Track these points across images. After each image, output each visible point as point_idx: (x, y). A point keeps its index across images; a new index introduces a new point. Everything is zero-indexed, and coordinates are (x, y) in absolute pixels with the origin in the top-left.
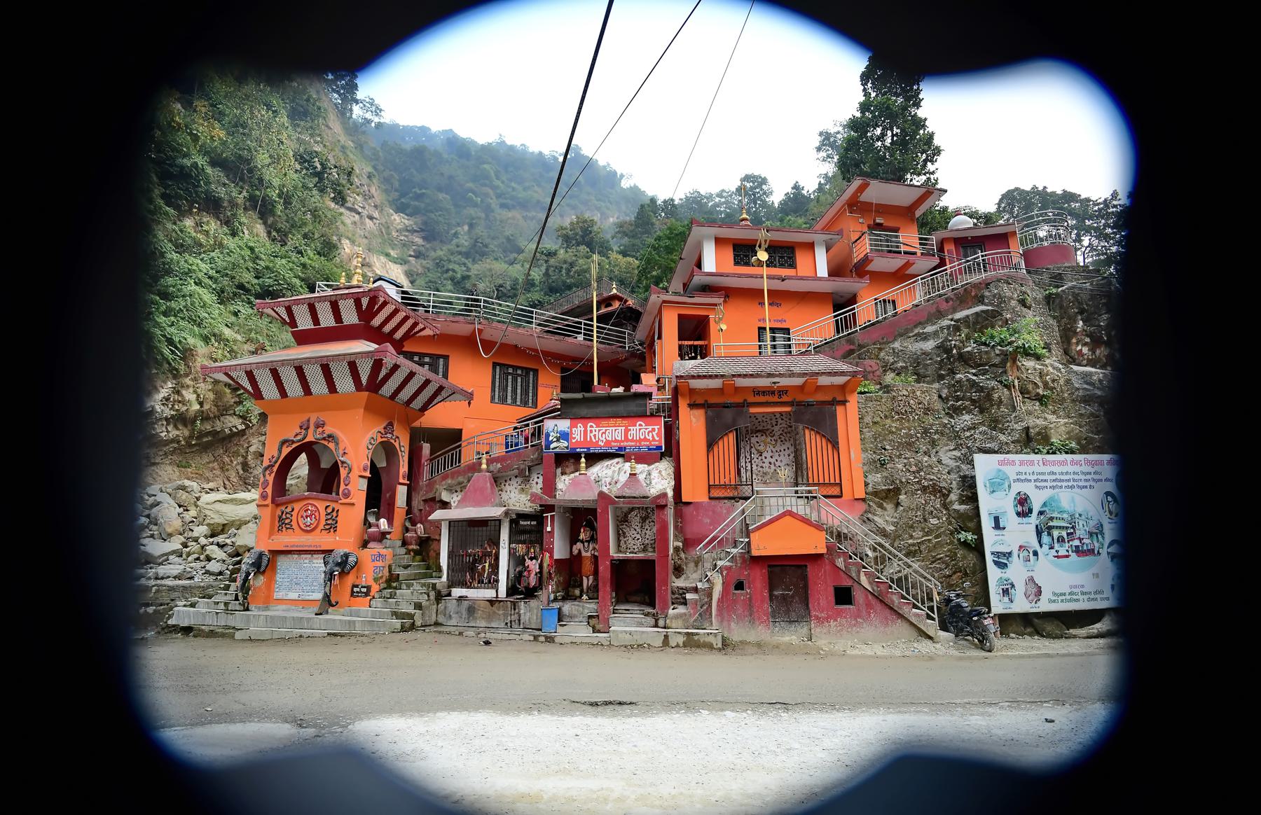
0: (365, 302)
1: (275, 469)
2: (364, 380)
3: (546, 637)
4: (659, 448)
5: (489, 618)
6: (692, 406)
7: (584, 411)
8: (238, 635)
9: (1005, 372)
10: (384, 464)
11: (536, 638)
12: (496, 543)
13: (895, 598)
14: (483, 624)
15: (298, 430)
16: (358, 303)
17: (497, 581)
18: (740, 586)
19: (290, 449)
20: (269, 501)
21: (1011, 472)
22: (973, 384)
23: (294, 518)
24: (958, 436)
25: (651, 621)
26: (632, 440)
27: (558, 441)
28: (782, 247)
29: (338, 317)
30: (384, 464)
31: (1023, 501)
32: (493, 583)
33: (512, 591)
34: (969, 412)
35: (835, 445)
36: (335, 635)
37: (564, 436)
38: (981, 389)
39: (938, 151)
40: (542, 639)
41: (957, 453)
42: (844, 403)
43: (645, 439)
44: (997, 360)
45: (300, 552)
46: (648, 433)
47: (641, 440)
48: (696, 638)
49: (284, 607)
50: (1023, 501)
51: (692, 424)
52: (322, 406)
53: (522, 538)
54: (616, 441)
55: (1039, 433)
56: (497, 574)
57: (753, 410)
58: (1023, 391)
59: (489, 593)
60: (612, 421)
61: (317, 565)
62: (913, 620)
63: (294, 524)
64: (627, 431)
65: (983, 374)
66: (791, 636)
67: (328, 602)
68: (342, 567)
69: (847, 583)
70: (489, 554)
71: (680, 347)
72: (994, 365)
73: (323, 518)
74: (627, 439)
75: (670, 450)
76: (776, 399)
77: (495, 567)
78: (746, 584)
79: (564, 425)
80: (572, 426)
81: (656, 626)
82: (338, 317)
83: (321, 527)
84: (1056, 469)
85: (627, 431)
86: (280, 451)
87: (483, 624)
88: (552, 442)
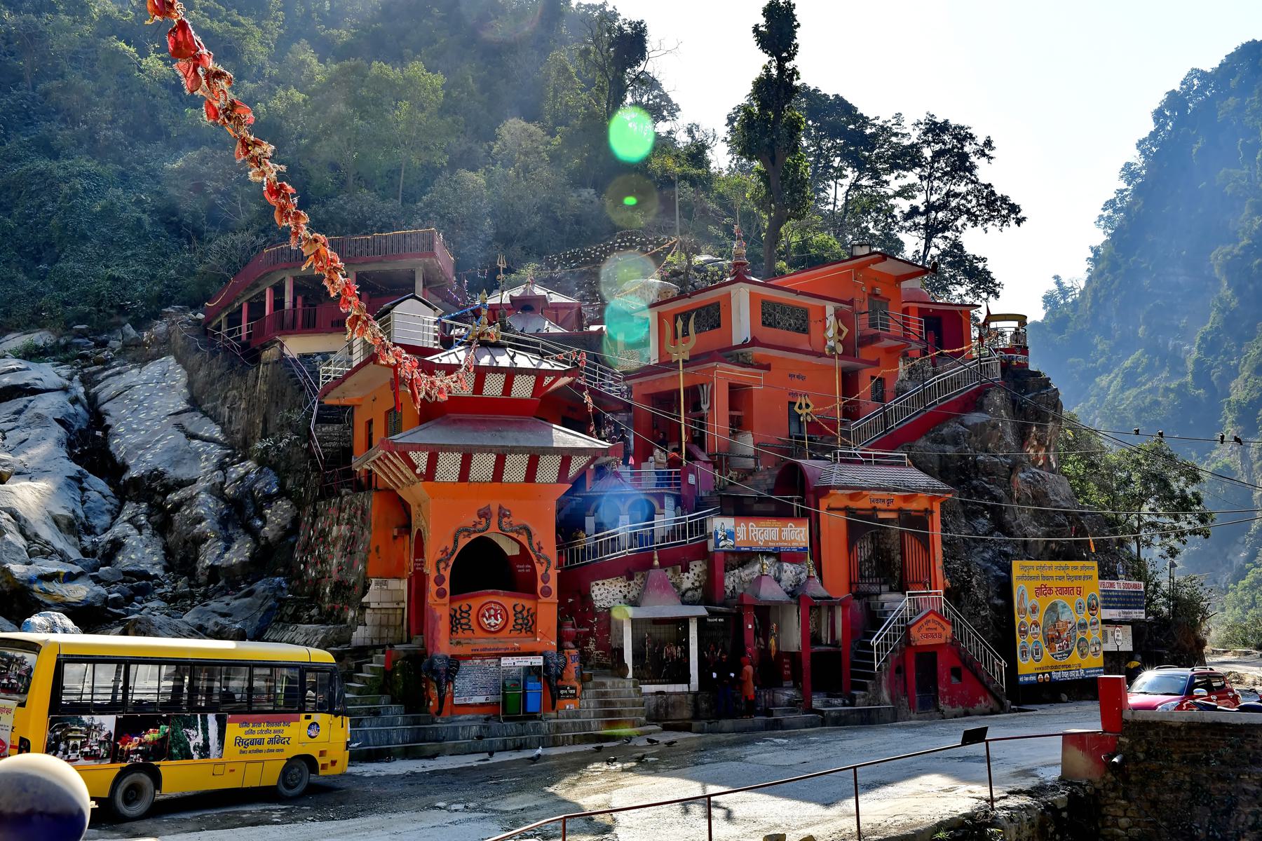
15: (477, 519)
19: (468, 540)
30: (517, 552)
32: (686, 679)
37: (730, 535)
43: (795, 541)
64: (781, 531)
71: (731, 417)
73: (512, 619)
79: (729, 523)
83: (510, 626)
85: (781, 531)
86: (456, 541)
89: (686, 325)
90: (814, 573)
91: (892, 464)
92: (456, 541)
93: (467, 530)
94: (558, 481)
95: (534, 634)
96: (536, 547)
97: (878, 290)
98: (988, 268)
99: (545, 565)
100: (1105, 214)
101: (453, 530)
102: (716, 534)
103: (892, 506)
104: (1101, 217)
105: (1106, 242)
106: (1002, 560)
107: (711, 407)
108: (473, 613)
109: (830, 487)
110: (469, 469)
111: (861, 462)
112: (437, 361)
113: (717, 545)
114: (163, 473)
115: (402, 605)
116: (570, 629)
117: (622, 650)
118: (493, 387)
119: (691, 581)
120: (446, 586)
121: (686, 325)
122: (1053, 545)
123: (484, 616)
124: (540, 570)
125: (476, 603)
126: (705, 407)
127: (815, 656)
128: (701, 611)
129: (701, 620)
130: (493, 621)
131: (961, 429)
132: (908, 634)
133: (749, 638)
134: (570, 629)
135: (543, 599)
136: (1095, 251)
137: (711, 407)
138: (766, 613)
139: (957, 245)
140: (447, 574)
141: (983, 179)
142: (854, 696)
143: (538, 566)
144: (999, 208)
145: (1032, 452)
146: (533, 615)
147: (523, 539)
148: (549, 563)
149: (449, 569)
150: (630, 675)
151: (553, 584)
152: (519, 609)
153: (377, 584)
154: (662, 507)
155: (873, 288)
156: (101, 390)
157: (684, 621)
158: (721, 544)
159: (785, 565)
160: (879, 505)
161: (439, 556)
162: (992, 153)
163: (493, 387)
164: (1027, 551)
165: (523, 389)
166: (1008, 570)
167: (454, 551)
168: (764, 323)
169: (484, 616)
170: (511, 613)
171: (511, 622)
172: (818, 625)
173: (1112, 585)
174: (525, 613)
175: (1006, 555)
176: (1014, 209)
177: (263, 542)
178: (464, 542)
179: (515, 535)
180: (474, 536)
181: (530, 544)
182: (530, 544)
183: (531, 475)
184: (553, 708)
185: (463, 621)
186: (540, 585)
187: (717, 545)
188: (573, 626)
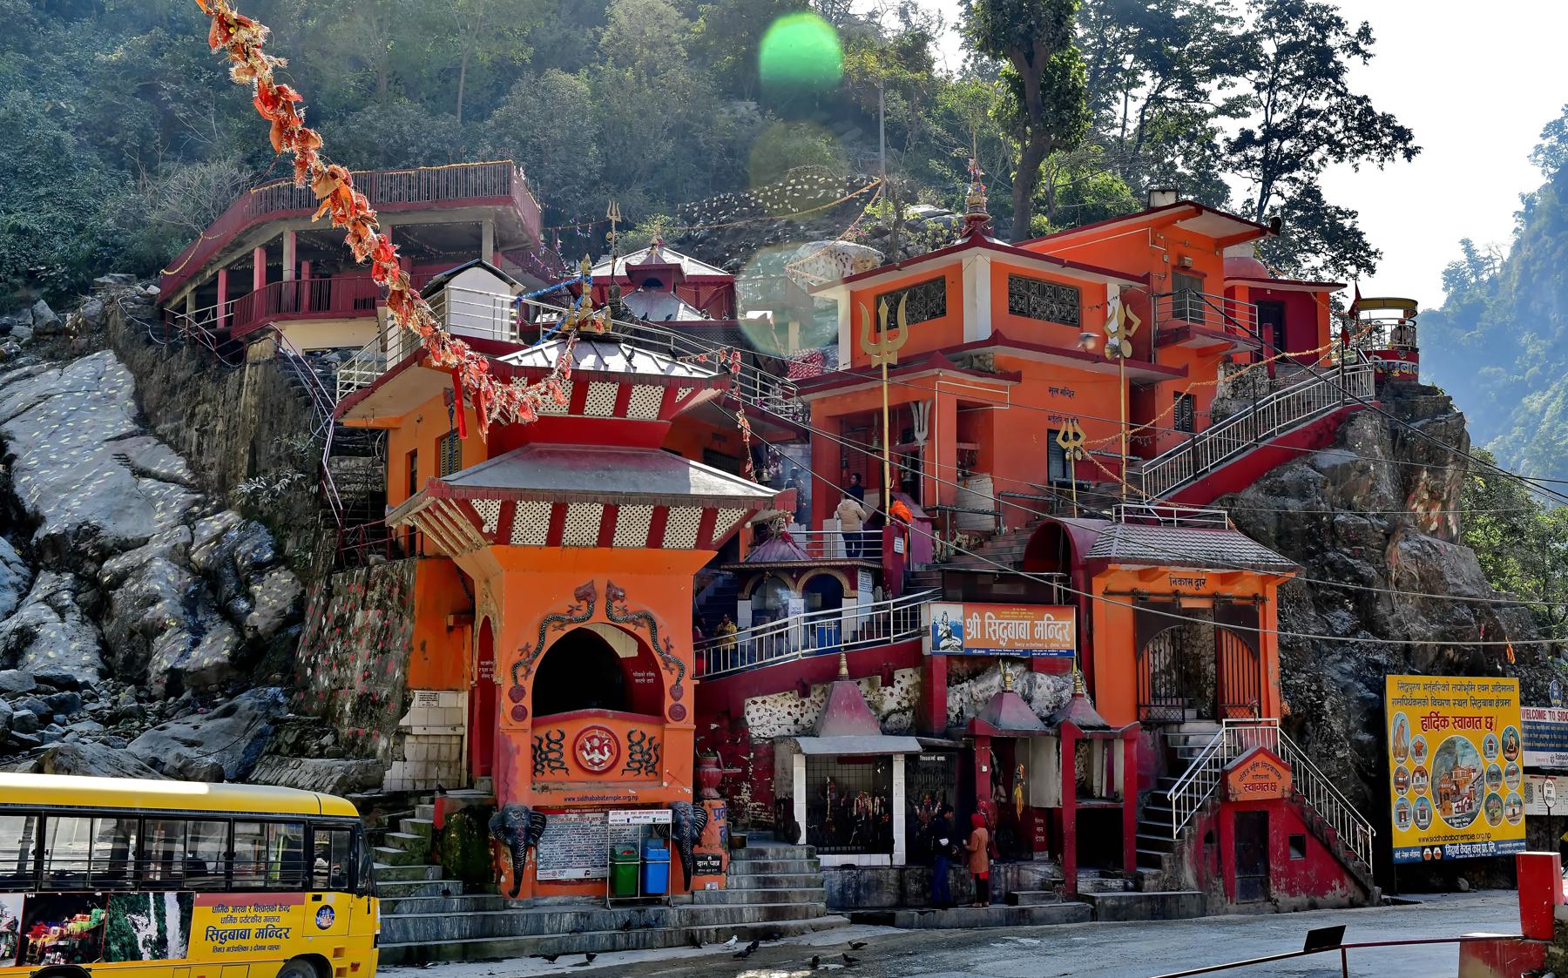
1: (534, 668)
15: (575, 603)
19: (560, 634)
23: (567, 750)
26: (1039, 641)
27: (949, 636)
37: (956, 630)
42: (1263, 600)
54: (1021, 640)
64: (1033, 626)
74: (1033, 639)
85: (1033, 626)
86: (542, 635)
89: (893, 312)
90: (1082, 690)
91: (1204, 527)
92: (542, 635)
93: (558, 619)
94: (697, 546)
95: (659, 776)
96: (662, 646)
97: (1188, 261)
98: (1360, 227)
99: (676, 673)
100: (1546, 143)
101: (537, 618)
102: (935, 628)
103: (1202, 590)
104: (1539, 148)
105: (1546, 186)
106: (1370, 674)
107: (930, 437)
108: (567, 744)
109: (1108, 560)
111: (1158, 523)
112: (514, 363)
113: (936, 646)
114: (97, 529)
115: (460, 731)
117: (789, 803)
118: (600, 403)
120: (527, 702)
121: (893, 312)
122: (1451, 652)
123: (583, 748)
124: (669, 680)
126: (920, 436)
127: (1082, 814)
128: (912, 744)
129: (911, 758)
130: (596, 756)
132: (1223, 777)
133: (983, 786)
135: (672, 724)
136: (1529, 201)
137: (930, 437)
138: (1008, 749)
139: (1312, 192)
140: (528, 684)
141: (1355, 89)
143: (665, 673)
144: (1378, 133)
145: (1420, 509)
146: (658, 748)
147: (644, 632)
148: (682, 670)
149: (531, 677)
151: (688, 701)
152: (636, 738)
153: (422, 699)
154: (854, 587)
155: (1181, 257)
157: (886, 760)
158: (942, 644)
160: (1184, 588)
161: (516, 657)
162: (1370, 49)
163: (600, 403)
164: (1408, 660)
165: (644, 406)
166: (1380, 688)
167: (538, 650)
168: (1012, 310)
169: (583, 748)
170: (625, 744)
171: (625, 758)
172: (1088, 768)
173: (1541, 715)
174: (645, 745)
175: (1377, 666)
176: (1402, 135)
177: (249, 635)
178: (553, 636)
180: (568, 628)
181: (654, 641)
182: (654, 641)
183: (656, 537)
184: (687, 888)
186: (668, 702)
187: (936, 646)
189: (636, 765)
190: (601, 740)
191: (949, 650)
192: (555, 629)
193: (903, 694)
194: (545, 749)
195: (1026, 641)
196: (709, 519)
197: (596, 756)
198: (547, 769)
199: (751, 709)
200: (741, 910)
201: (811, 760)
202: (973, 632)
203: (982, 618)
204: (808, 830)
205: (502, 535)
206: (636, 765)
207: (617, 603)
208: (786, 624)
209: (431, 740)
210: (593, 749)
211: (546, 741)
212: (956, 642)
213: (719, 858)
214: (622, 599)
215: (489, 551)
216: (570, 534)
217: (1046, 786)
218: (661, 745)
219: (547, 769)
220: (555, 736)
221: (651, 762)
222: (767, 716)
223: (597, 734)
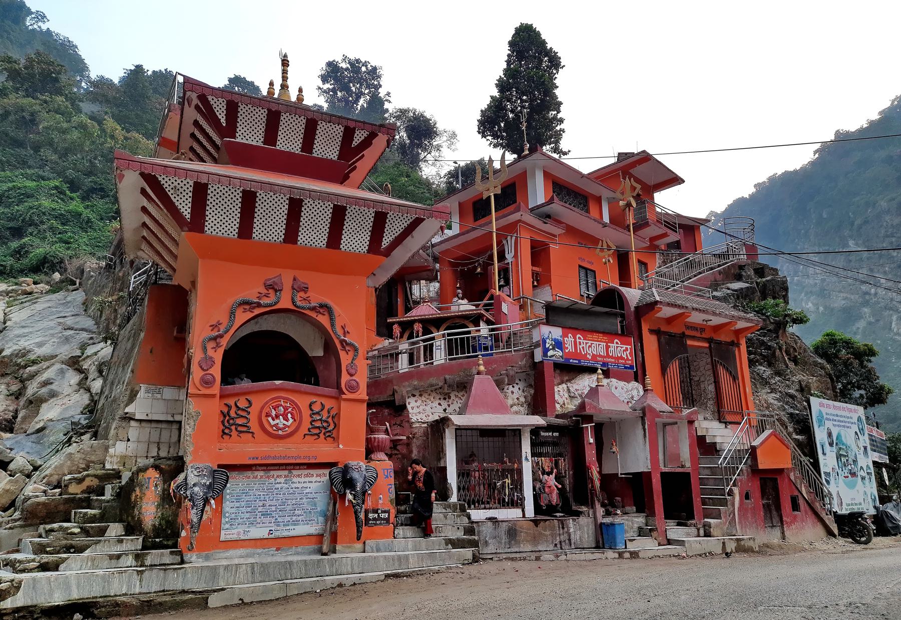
0: (359, 137)
1: (225, 342)
2: (386, 242)
3: (631, 553)
4: (631, 367)
5: (535, 539)
6: (652, 331)
7: (570, 322)
8: (214, 601)
9: (777, 337)
10: (320, 353)
11: (621, 555)
12: (517, 456)
13: (817, 504)
14: (529, 548)
15: (264, 291)
16: (349, 133)
17: (522, 499)
18: (747, 497)
20: (216, 389)
21: (824, 410)
22: (763, 343)
24: (767, 383)
25: (693, 530)
26: (612, 357)
27: (553, 349)
28: (580, 195)
29: (271, 135)
30: (320, 353)
31: (830, 435)
32: (518, 503)
33: (538, 509)
34: (761, 364)
35: (735, 378)
36: (396, 576)
37: (558, 345)
38: (769, 348)
39: (374, 73)
40: (627, 555)
41: (773, 395)
42: (738, 345)
43: (622, 358)
44: (771, 327)
45: (267, 467)
46: (621, 350)
47: (618, 358)
48: (742, 543)
49: (241, 551)
50: (830, 435)
51: (651, 343)
52: (311, 261)
53: (544, 450)
54: (600, 356)
55: (806, 386)
56: (521, 490)
57: (689, 342)
58: (788, 353)
59: (513, 514)
60: (595, 336)
61: (313, 485)
62: (827, 522)
63: (254, 425)
64: (608, 347)
65: (764, 336)
66: (773, 537)
67: (327, 542)
68: (343, 483)
69: (796, 493)
70: (511, 471)
72: (769, 331)
74: (608, 356)
75: (638, 374)
76: (698, 334)
77: (518, 485)
78: (751, 495)
79: (556, 332)
80: (565, 335)
81: (699, 536)
82: (271, 135)
83: (304, 430)
84: (839, 413)
85: (608, 347)
86: (232, 314)
87: (529, 548)
88: (548, 350)
92: (232, 314)
94: (369, 251)
95: (336, 440)
96: (339, 332)
99: (351, 353)
101: (231, 301)
102: (544, 342)
103: (704, 336)
107: (516, 256)
108: (254, 411)
110: (251, 223)
114: (29, 351)
116: (382, 436)
117: (445, 468)
118: (289, 140)
119: (515, 396)
120: (216, 371)
123: (268, 415)
124: (345, 358)
125: (258, 402)
126: (509, 257)
127: (663, 474)
128: (538, 420)
129: (535, 431)
130: (281, 422)
131: (729, 292)
134: (382, 436)
140: (218, 357)
142: (709, 526)
143: (342, 354)
147: (324, 320)
148: (356, 350)
149: (221, 351)
150: (454, 499)
151: (362, 378)
152: (316, 408)
153: (147, 392)
156: (310, 554)
157: (515, 433)
158: (550, 353)
159: (614, 381)
160: (688, 332)
169: (268, 415)
170: (306, 413)
171: (306, 425)
179: (313, 314)
181: (332, 325)
182: (332, 325)
184: (359, 538)
185: (240, 421)
186: (345, 378)
188: (386, 432)
189: (317, 431)
190: (286, 409)
191: (554, 358)
192: (245, 311)
193: (520, 392)
194: (233, 414)
195: (604, 357)
196: (380, 220)
197: (281, 422)
198: (234, 433)
199: (556, 389)
200: (407, 557)
201: (459, 429)
202: (569, 347)
203: (575, 338)
204: (459, 489)
205: (197, 222)
206: (317, 431)
207: (302, 294)
208: (433, 339)
209: (154, 425)
210: (277, 417)
211: (234, 409)
212: (559, 353)
213: (388, 512)
214: (305, 289)
215: (183, 236)
216: (258, 233)
217: (635, 457)
218: (338, 415)
219: (234, 433)
220: (242, 404)
221: (327, 429)
222: (422, 411)
223: (280, 405)
